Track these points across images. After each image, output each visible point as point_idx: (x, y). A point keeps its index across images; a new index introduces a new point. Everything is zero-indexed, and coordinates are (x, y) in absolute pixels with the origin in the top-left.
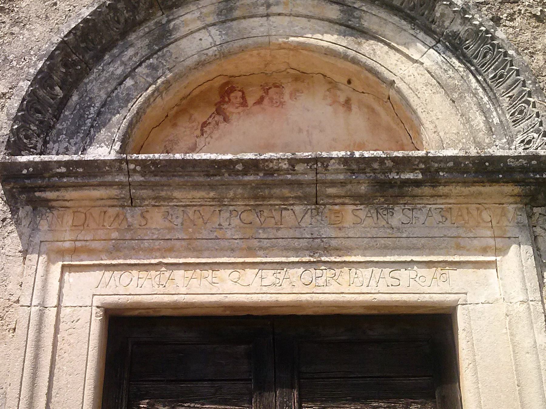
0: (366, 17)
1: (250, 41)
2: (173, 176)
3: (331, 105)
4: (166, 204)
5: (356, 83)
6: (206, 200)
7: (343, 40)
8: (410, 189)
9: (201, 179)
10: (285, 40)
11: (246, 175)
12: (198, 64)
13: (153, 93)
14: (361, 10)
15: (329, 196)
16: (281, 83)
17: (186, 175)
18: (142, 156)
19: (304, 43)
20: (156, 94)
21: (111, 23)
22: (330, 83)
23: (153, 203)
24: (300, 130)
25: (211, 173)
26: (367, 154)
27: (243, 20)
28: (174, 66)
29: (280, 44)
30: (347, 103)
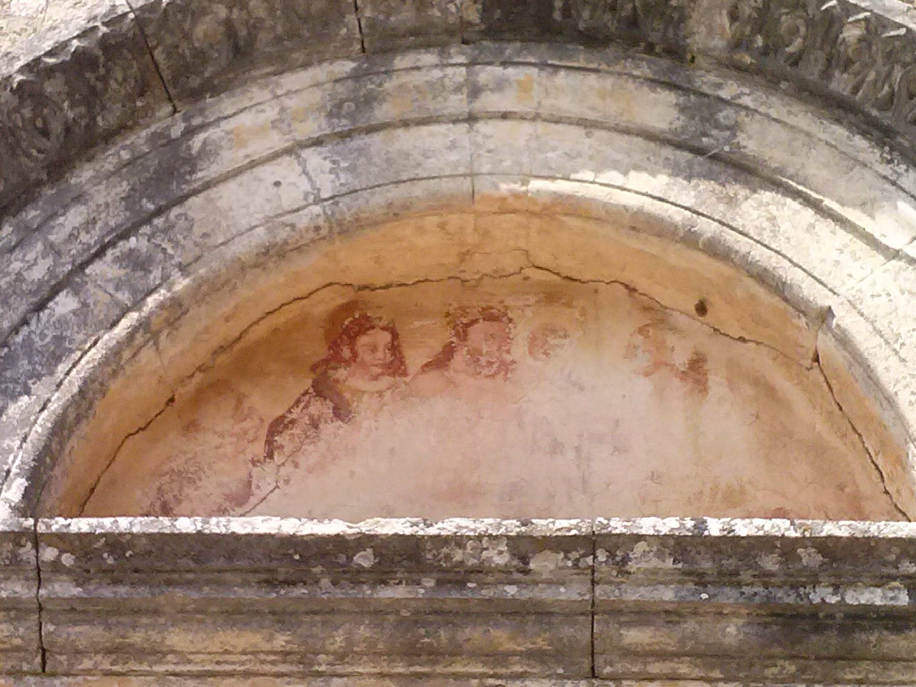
0: (752, 125)
1: (418, 190)
2: (169, 583)
3: (647, 374)
4: (145, 667)
5: (720, 312)
6: (262, 657)
7: (684, 188)
8: (873, 638)
9: (250, 595)
10: (517, 187)
11: (384, 582)
12: (266, 254)
13: (131, 335)
14: (739, 105)
15: (630, 653)
16: (507, 308)
17: (207, 582)
18: (81, 525)
19: (570, 197)
20: (139, 338)
21: (24, 135)
22: (647, 309)
23: (106, 665)
24: (556, 448)
25: (281, 577)
26: (744, 528)
27: (400, 132)
28: (197, 259)
29: (504, 199)
30: (696, 367)
